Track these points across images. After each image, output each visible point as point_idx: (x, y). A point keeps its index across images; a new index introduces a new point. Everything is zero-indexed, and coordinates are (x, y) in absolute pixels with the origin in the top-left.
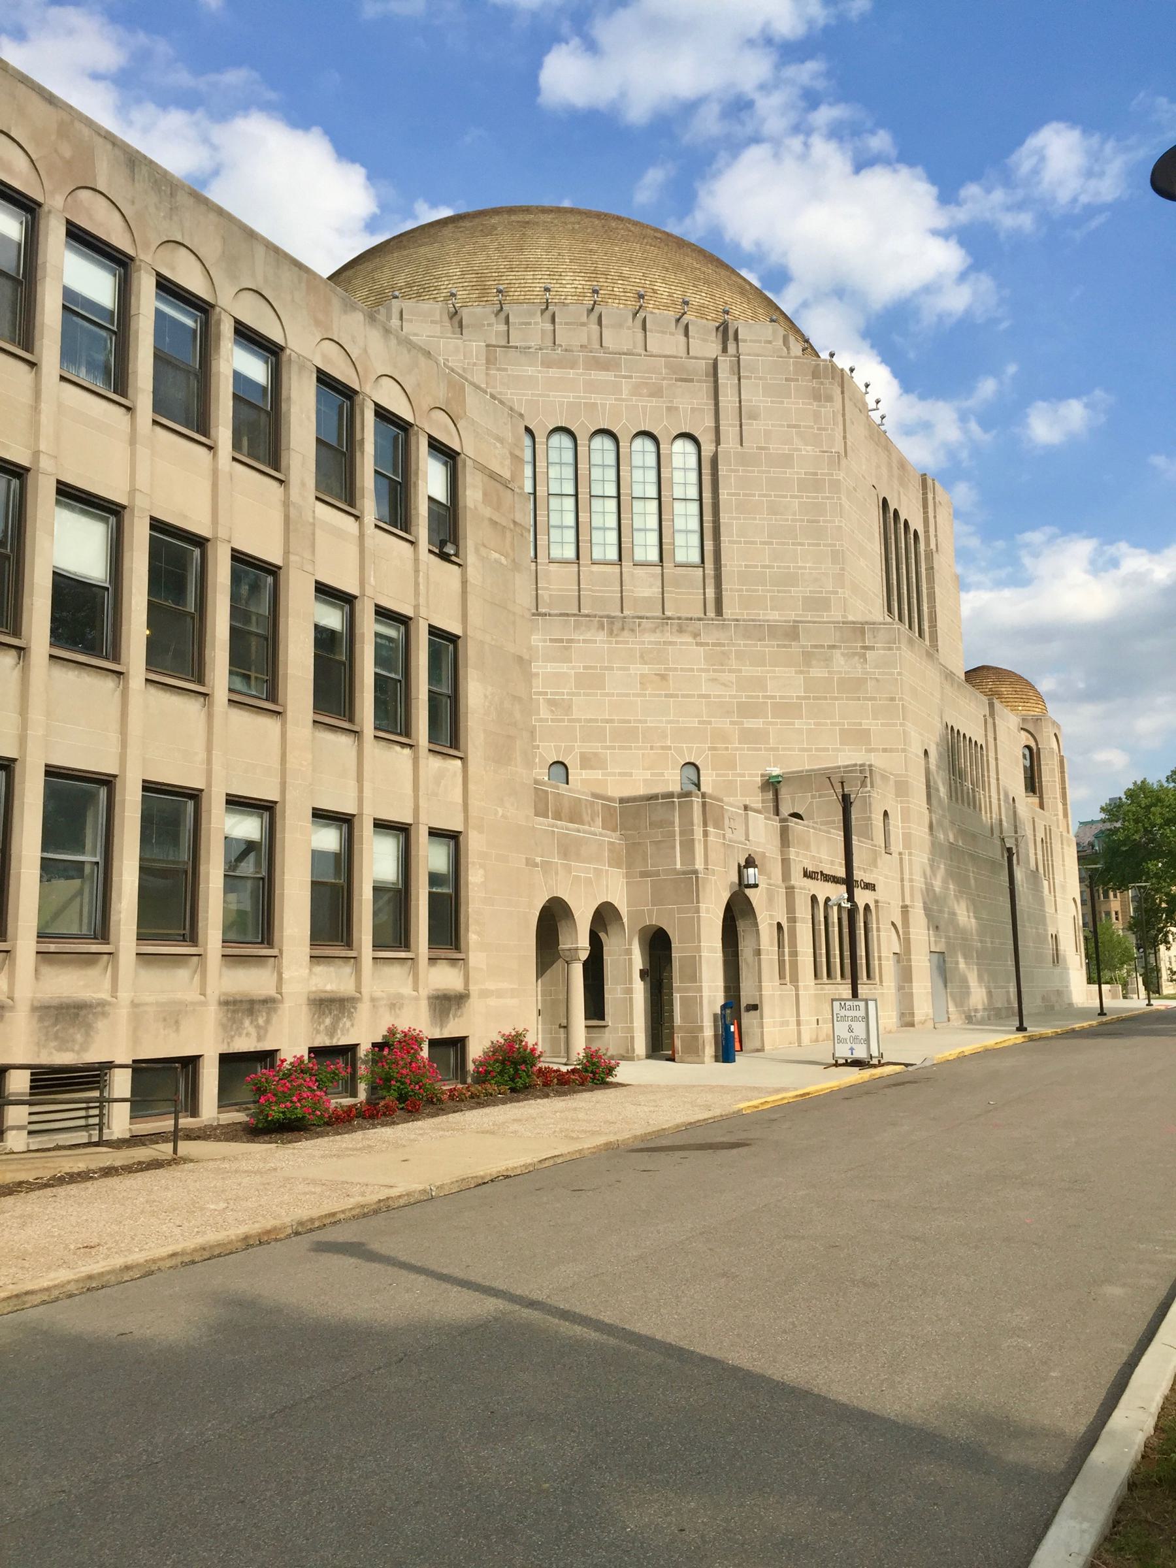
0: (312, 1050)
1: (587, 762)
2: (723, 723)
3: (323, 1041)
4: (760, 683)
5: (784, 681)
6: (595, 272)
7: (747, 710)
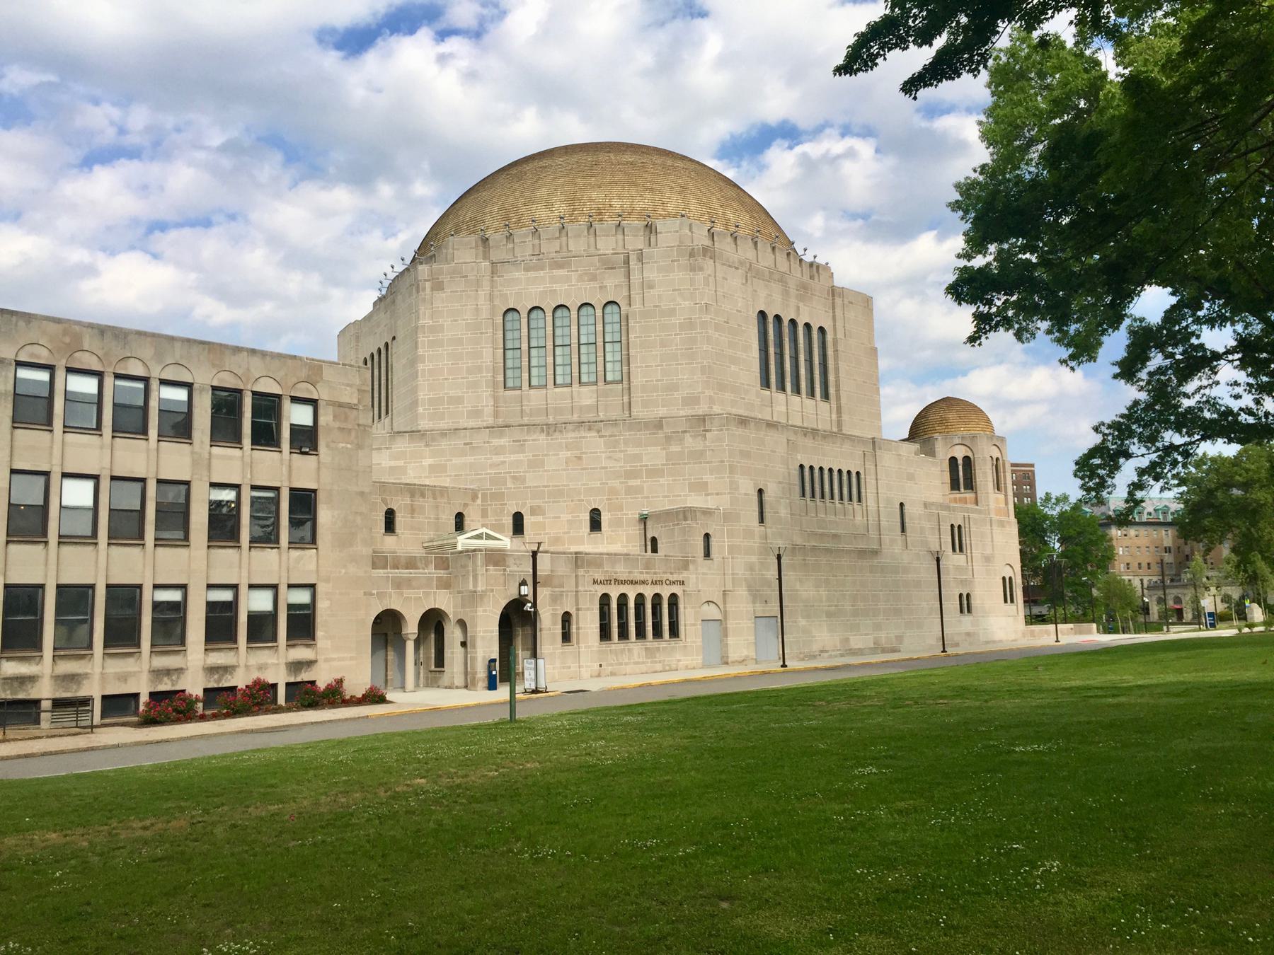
0: (206, 690)
1: (534, 511)
2: (616, 484)
3: (212, 685)
4: (638, 457)
5: (654, 455)
6: (574, 199)
7: (631, 474)
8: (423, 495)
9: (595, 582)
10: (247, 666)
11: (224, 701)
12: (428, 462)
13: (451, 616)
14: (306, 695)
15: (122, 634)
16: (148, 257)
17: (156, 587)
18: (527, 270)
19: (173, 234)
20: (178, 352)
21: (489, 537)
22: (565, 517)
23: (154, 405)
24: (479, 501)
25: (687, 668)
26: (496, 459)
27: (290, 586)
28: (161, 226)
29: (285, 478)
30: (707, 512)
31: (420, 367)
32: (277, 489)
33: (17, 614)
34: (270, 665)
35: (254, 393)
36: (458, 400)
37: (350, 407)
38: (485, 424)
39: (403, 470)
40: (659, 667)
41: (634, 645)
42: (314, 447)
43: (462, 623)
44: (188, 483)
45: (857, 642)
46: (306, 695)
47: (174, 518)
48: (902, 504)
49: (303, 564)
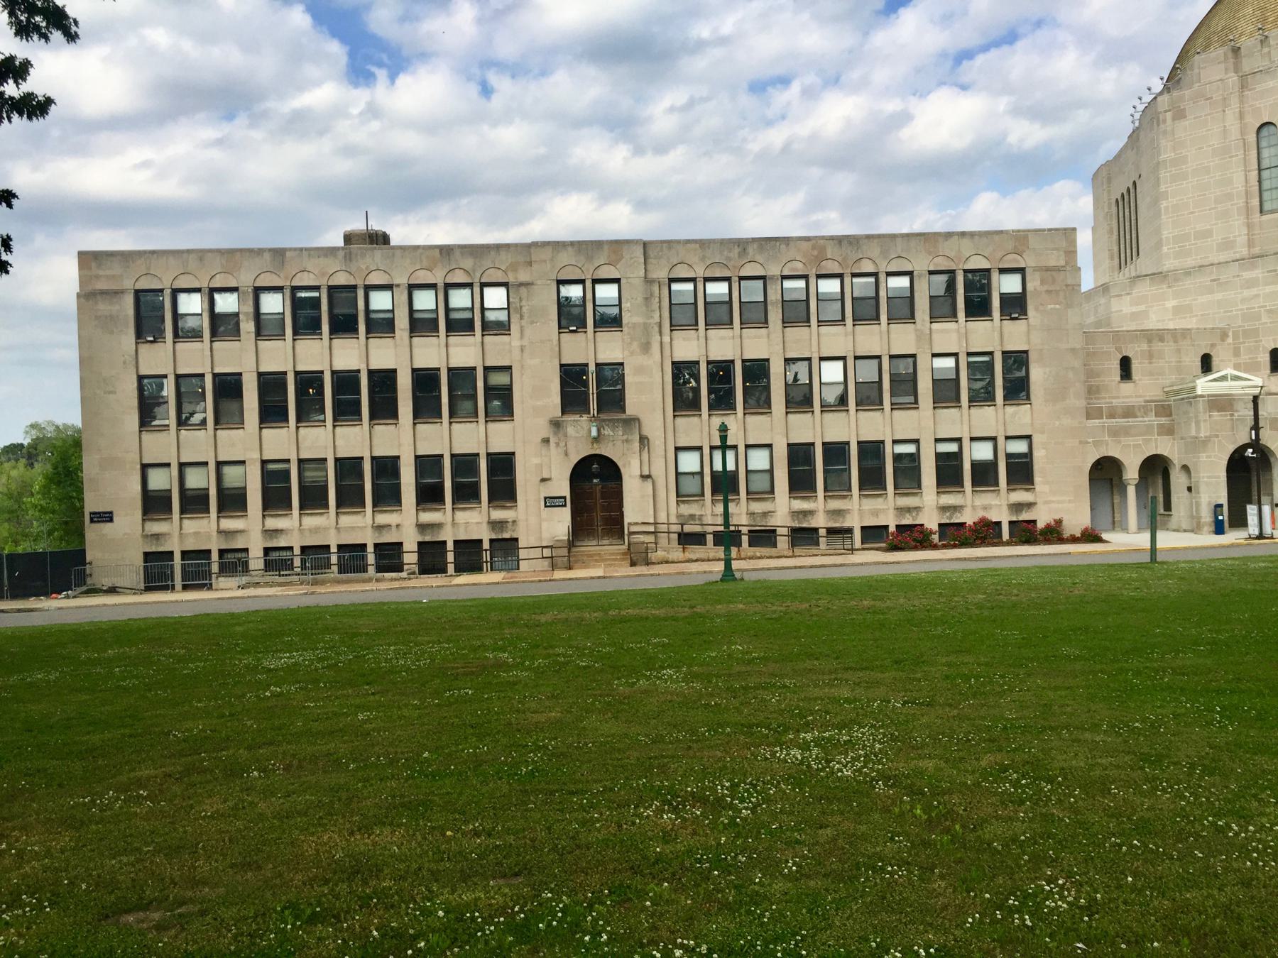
0: (940, 525)
8: (1162, 339)
10: (974, 507)
11: (955, 534)
12: (1171, 304)
13: (1176, 462)
14: (1025, 533)
15: (872, 480)
16: (956, 89)
17: (895, 442)
19: (980, 59)
20: (899, 247)
21: (1236, 378)
23: (882, 294)
24: (1230, 340)
27: (1007, 438)
28: (966, 55)
29: (997, 342)
31: (1164, 204)
32: (991, 353)
33: (798, 465)
34: (995, 505)
35: (966, 271)
36: (1207, 234)
37: (1058, 269)
38: (1238, 256)
39: (1144, 314)
42: (1024, 312)
43: (1185, 468)
44: (914, 356)
46: (1025, 533)
47: (905, 385)
49: (1018, 417)
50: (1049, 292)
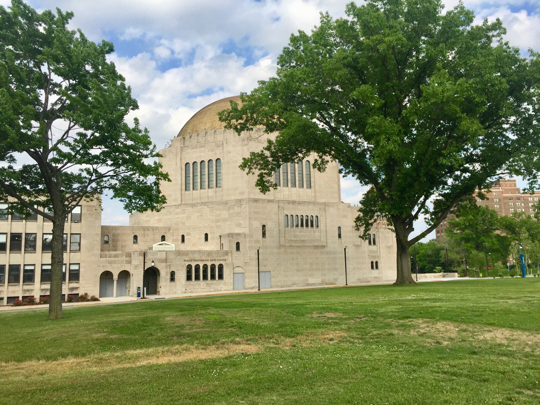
1: (188, 234)
5: (225, 214)
7: (217, 221)
8: (148, 230)
9: (185, 261)
12: (156, 218)
15: (14, 279)
17: (25, 265)
18: (192, 149)
22: (197, 236)
24: (171, 231)
25: (225, 290)
26: (176, 216)
30: (238, 235)
40: (212, 290)
41: (202, 282)
45: (311, 280)
48: (340, 227)
50: (90, 214)
